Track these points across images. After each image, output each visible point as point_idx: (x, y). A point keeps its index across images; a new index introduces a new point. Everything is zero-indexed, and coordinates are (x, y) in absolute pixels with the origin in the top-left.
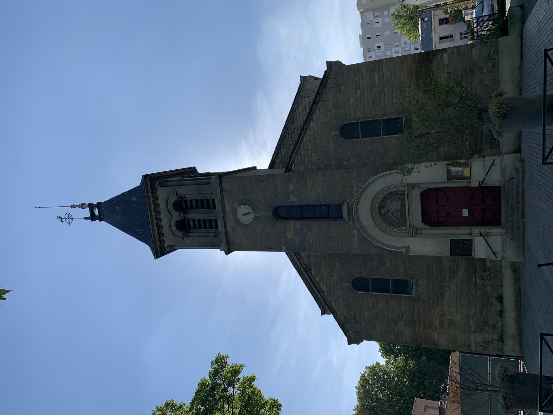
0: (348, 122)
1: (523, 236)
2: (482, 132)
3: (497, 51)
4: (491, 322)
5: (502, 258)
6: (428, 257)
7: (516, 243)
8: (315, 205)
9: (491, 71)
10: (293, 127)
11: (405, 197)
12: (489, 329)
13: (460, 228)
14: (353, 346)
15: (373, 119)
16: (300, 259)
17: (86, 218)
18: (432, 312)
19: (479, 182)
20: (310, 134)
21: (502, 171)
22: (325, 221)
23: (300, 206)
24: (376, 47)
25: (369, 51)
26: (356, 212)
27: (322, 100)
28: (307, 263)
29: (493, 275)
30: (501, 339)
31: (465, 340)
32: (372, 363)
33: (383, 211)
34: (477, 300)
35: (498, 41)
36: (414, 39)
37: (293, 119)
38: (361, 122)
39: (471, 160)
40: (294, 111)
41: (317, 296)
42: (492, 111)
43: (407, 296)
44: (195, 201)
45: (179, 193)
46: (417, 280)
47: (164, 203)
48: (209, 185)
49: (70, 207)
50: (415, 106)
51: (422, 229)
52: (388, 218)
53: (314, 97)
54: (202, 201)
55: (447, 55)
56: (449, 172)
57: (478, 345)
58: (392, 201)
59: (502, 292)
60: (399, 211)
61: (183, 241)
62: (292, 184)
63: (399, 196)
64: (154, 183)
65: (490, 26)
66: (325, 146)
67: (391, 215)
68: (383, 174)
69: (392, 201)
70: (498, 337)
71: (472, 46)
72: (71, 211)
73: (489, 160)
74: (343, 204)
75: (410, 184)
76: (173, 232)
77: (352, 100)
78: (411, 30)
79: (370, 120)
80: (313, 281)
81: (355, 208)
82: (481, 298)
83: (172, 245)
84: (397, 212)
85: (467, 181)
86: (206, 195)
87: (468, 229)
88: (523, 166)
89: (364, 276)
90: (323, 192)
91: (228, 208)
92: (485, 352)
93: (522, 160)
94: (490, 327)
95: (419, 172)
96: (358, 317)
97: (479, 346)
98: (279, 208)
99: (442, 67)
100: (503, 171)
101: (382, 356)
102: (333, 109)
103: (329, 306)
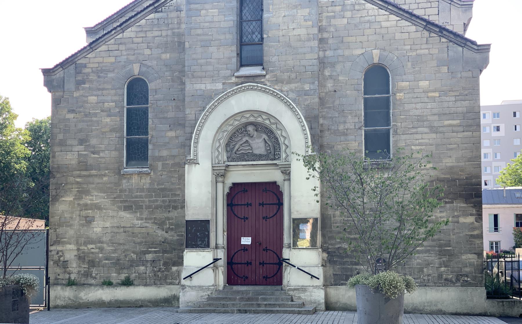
0: (391, 77)
1: (214, 311)
3: (465, 284)
4: (94, 271)
5: (184, 286)
6: (183, 191)
7: (204, 303)
9: (440, 276)
11: (271, 160)
13: (226, 234)
14: (41, 78)
15: (391, 115)
19: (289, 260)
21: (303, 287)
22: (237, 39)
24: (498, 125)
25: (494, 114)
26: (250, 88)
27: (431, 36)
28: (167, 5)
29: (159, 274)
30: (71, 283)
31: (66, 238)
32: (15, 108)
33: (250, 128)
35: (482, 287)
36: (501, 180)
38: (388, 99)
39: (320, 250)
41: (114, 22)
42: (388, 275)
43: (123, 160)
46: (149, 174)
50: (405, 176)
51: (223, 183)
52: (240, 135)
53: (437, 22)
56: (305, 221)
57: (60, 254)
58: (266, 142)
59: (137, 285)
60: (251, 151)
63: (273, 152)
65: (503, 278)
66: (356, 39)
67: (244, 140)
70: (74, 279)
71: (480, 254)
73: (319, 272)
74: (263, 68)
75: (290, 167)
77: (424, 84)
78: (516, 175)
79: (391, 111)
80: (139, 16)
81: (256, 88)
84: (249, 149)
85: (290, 244)
87: (223, 244)
88: (308, 312)
89: (150, 98)
90: (283, 36)
92: (51, 263)
93: (315, 311)
95: (308, 179)
96: (87, 86)
99: (456, 214)
100: (303, 289)
101: (28, 123)
102: (414, 53)
103: (100, 40)
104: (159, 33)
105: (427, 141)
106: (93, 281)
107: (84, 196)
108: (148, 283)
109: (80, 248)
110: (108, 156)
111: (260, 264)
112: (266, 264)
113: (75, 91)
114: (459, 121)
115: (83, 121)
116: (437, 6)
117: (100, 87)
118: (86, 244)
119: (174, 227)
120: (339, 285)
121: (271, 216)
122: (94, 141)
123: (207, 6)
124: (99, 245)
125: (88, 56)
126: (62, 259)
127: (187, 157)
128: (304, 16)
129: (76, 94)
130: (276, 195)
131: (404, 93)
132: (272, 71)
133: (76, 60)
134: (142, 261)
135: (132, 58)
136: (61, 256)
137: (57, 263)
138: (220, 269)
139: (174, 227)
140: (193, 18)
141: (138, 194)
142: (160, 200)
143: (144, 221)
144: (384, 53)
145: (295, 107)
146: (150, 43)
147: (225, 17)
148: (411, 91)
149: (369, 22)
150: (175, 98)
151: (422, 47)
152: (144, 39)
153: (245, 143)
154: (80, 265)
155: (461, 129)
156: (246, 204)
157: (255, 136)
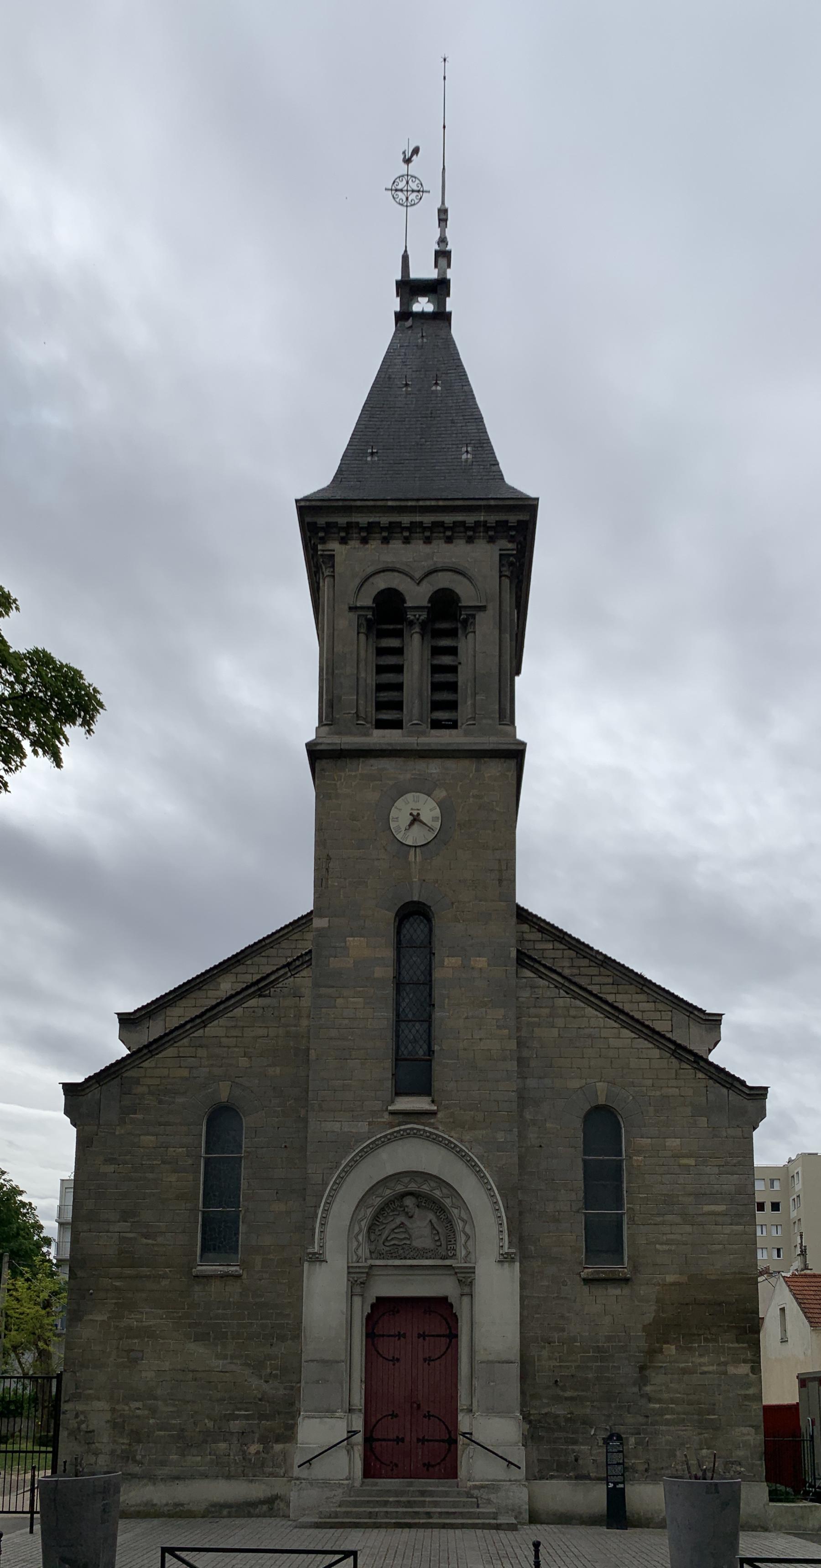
2: (575, 1442)
4: (140, 1451)
8: (430, 1026)
11: (441, 1258)
12: (123, 1444)
15: (625, 1192)
16: (291, 968)
17: (405, 258)
18: (160, 1311)
19: (471, 1434)
20: (604, 1028)
23: (431, 981)
28: (278, 986)
31: (91, 1389)
33: (409, 1202)
34: (192, 1420)
37: (624, 982)
40: (642, 989)
41: (169, 1006)
45: (480, 617)
46: (239, 1277)
47: (454, 560)
48: (498, 716)
49: (443, 203)
54: (453, 687)
55: (746, 1373)
57: (82, 1417)
60: (408, 1242)
61: (346, 607)
62: (489, 965)
63: (444, 1246)
64: (512, 536)
66: (572, 1063)
67: (398, 1221)
68: (502, 1210)
69: (434, 1228)
73: (518, 1455)
74: (433, 1102)
75: (474, 1273)
76: (371, 576)
77: (673, 1143)
79: (625, 1185)
82: (198, 1430)
83: (333, 566)
86: (469, 703)
87: (361, 1405)
91: (434, 768)
94: (127, 1447)
96: (139, 1116)
98: (425, 921)
99: (722, 1359)
100: (492, 1487)
102: (658, 1093)
104: (264, 1032)
106: (138, 1468)
108: (232, 1474)
109: (117, 1407)
111: (418, 1440)
112: (428, 1441)
113: (118, 1125)
116: (669, 1018)
120: (547, 1479)
121: (436, 1357)
126: (83, 1426)
127: (307, 1248)
128: (498, 1020)
130: (446, 1320)
131: (645, 1157)
134: (222, 1433)
136: (83, 1422)
138: (355, 1448)
140: (323, 1010)
143: (229, 1361)
145: (483, 1169)
146: (248, 1048)
149: (590, 1036)
150: (287, 1145)
152: (239, 1039)
153: (398, 1227)
154: (116, 1439)
156: (397, 1333)
157: (416, 1216)
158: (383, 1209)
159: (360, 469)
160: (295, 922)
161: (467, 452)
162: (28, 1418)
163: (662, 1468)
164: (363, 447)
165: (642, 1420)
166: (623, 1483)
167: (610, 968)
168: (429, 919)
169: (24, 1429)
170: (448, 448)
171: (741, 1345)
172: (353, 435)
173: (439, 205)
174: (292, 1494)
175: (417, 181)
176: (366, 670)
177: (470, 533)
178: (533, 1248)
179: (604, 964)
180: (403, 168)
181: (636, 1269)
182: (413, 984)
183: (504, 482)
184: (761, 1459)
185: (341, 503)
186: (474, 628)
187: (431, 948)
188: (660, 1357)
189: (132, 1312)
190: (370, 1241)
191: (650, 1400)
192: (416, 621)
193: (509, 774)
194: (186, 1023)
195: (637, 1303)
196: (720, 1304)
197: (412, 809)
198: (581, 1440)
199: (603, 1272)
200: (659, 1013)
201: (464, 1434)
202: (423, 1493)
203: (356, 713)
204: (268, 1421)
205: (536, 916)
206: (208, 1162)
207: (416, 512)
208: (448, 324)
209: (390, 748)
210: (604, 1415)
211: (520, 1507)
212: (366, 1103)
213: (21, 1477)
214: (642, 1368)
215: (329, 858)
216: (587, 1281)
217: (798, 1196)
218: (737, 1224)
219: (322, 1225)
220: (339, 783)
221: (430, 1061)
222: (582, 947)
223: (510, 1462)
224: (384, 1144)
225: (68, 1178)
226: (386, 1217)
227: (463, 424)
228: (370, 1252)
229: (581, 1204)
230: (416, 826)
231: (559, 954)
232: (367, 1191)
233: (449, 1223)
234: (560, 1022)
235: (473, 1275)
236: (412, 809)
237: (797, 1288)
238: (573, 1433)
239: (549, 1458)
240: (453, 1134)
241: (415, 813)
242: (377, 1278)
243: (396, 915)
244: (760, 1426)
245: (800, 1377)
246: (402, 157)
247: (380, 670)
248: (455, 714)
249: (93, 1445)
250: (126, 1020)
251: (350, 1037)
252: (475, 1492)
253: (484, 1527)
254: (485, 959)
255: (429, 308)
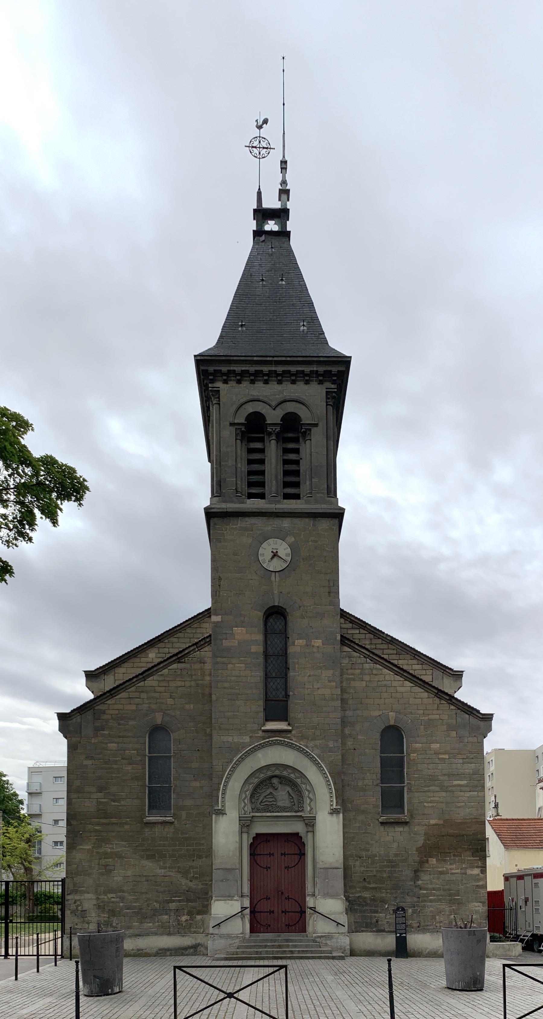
2: (377, 912)
10: (392, 652)
11: (295, 812)
15: (405, 774)
17: (259, 194)
23: (286, 654)
28: (190, 656)
33: (275, 781)
37: (404, 653)
40: (414, 657)
41: (117, 667)
43: (145, 809)
44: (298, 458)
45: (314, 430)
46: (172, 823)
49: (284, 157)
54: (297, 473)
55: (477, 873)
57: (78, 903)
58: (290, 795)
60: (275, 803)
61: (228, 423)
62: (323, 644)
63: (296, 804)
64: (334, 380)
67: (268, 792)
69: (290, 795)
72: (275, 157)
73: (343, 919)
75: (315, 819)
77: (435, 746)
79: (405, 770)
80: (162, 665)
82: (150, 908)
83: (219, 398)
86: (308, 483)
90: (308, 694)
91: (286, 523)
97: (76, 904)
98: (282, 618)
100: (329, 936)
102: (427, 718)
104: (183, 684)
105: (437, 799)
107: (103, 844)
108: (172, 932)
109: (100, 897)
110: (129, 804)
111: (283, 912)
113: (94, 737)
114: (466, 782)
115: (102, 769)
116: (431, 673)
117: (121, 734)
118: (105, 893)
119: (198, 876)
122: (113, 789)
123: (234, 661)
124: (119, 894)
125: (108, 702)
129: (93, 741)
130: (297, 845)
132: (298, 727)
133: (95, 705)
135: (154, 707)
136: (79, 905)
137: (74, 912)
138: (246, 916)
139: (198, 876)
140: (220, 671)
141: (162, 842)
142: (184, 849)
144: (399, 716)
145: (321, 762)
146: (172, 693)
147: (251, 672)
148: (423, 752)
151: (434, 713)
152: (167, 688)
155: (468, 789)
157: (279, 789)
158: (259, 785)
159: (235, 336)
160: (195, 617)
161: (304, 325)
162: (21, 905)
163: (428, 925)
164: (236, 321)
165: (416, 899)
166: (405, 933)
167: (395, 645)
168: (285, 618)
169: (19, 912)
170: (291, 323)
171: (475, 858)
172: (229, 313)
173: (281, 158)
174: (209, 942)
175: (266, 141)
176: (241, 463)
177: (307, 378)
178: (350, 805)
179: (391, 642)
180: (256, 132)
181: (412, 817)
182: (275, 656)
183: (328, 345)
184: (486, 920)
185: (224, 358)
186: (310, 437)
187: (286, 634)
188: (427, 865)
189: (108, 843)
190: (252, 802)
191: (421, 889)
192: (273, 432)
193: (334, 528)
194: (133, 678)
195: (412, 835)
196: (463, 836)
197: (273, 549)
198: (379, 911)
199: (392, 819)
200: (425, 671)
201: (311, 908)
202: (287, 941)
203: (236, 489)
204: (192, 903)
205: (348, 613)
206: (150, 758)
207: (272, 364)
208: (288, 239)
209: (258, 511)
210: (393, 897)
211: (344, 948)
212: (247, 725)
213: (31, 937)
214: (416, 871)
215: (220, 579)
216: (382, 823)
217: (492, 774)
218: (473, 791)
219: (223, 794)
220: (225, 532)
221: (287, 701)
222: (377, 632)
223: (339, 923)
224: (259, 749)
225: (32, 766)
226: (261, 789)
227: (301, 307)
228: (252, 808)
229: (379, 781)
230: (275, 559)
231: (363, 636)
232: (250, 775)
233: (300, 793)
234: (367, 678)
235: (314, 821)
236: (273, 549)
237: (497, 827)
238: (375, 907)
239: (361, 921)
240: (301, 743)
241: (275, 551)
242: (256, 822)
243: (264, 614)
244: (485, 902)
245: (505, 875)
246: (256, 124)
247: (250, 462)
248: (298, 490)
249: (86, 918)
250: (91, 676)
251: (237, 687)
252: (318, 940)
253: (328, 958)
254: (320, 641)
255: (276, 228)
